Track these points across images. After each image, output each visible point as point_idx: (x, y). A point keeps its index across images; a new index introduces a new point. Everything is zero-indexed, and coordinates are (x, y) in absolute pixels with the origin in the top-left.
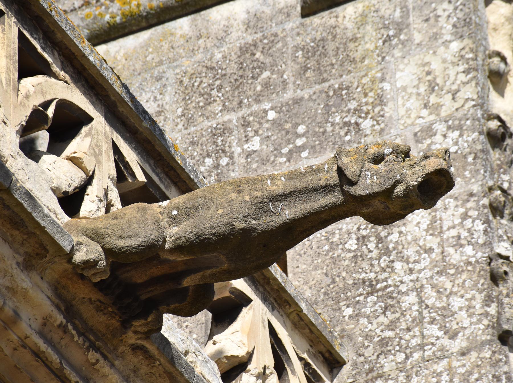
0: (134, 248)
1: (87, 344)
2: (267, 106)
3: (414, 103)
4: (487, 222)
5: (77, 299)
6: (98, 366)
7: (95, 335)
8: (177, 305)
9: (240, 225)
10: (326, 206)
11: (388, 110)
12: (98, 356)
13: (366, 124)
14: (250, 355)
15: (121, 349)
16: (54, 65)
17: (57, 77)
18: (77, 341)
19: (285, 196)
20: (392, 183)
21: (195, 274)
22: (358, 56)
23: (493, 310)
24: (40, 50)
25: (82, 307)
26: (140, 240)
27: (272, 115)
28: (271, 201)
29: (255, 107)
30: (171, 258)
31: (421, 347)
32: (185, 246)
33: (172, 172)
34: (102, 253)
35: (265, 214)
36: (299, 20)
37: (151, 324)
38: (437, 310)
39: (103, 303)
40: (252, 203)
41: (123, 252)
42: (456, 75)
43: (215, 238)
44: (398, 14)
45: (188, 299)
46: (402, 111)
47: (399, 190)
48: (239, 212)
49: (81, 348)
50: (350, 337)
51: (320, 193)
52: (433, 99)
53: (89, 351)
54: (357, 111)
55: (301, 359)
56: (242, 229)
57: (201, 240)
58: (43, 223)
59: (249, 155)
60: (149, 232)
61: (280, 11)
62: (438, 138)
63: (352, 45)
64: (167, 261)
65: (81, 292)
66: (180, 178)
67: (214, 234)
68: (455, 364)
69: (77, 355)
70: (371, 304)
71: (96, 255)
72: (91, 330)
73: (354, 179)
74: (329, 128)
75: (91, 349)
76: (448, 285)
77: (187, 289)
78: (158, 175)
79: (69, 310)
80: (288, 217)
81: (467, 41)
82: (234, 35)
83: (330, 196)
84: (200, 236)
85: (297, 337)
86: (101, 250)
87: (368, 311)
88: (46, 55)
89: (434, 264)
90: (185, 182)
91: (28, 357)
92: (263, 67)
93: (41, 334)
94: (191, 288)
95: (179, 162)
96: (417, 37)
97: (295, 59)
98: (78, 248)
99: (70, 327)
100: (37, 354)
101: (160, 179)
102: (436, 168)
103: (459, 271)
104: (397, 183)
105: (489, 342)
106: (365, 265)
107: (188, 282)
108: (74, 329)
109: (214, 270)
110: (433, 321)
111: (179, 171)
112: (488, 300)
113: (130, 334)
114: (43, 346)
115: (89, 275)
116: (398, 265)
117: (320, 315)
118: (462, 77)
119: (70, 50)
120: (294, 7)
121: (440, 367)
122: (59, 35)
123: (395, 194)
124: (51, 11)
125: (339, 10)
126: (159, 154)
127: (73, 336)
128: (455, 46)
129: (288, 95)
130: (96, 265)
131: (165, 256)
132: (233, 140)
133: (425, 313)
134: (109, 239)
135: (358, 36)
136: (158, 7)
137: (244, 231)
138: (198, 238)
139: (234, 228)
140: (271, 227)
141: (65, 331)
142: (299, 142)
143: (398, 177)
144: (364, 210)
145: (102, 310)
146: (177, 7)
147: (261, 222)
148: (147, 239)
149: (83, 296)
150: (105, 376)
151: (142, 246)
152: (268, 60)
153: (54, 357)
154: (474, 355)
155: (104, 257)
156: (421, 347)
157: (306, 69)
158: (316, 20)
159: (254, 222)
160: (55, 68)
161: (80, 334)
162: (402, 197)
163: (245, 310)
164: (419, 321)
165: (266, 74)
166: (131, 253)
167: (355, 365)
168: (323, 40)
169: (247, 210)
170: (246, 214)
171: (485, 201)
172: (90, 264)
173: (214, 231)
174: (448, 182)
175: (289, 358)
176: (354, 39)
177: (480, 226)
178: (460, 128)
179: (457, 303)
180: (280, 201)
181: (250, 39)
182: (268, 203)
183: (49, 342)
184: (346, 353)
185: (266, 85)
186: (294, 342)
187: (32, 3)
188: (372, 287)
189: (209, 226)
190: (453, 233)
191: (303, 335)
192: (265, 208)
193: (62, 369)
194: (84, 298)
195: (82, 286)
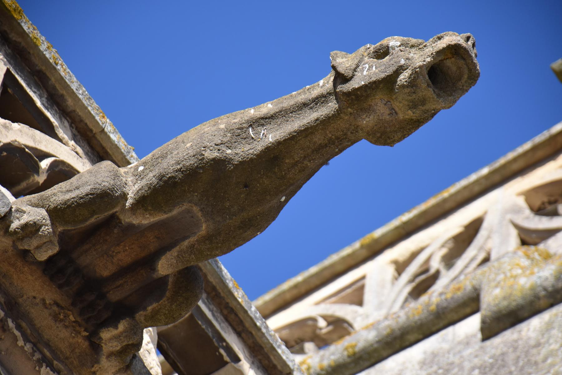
0: (81, 198)
1: (37, 356)
5: (25, 297)
7: (52, 351)
8: (155, 305)
9: (209, 155)
10: (317, 120)
16: (61, 131)
17: (60, 140)
18: (22, 347)
19: (269, 118)
20: (395, 69)
21: (170, 250)
22: (540, 358)
24: (39, 103)
25: (33, 310)
26: (89, 187)
28: (251, 126)
30: (135, 221)
32: (148, 196)
33: (232, 316)
34: (47, 217)
35: (244, 142)
36: (480, 344)
37: (124, 334)
39: (62, 308)
41: (69, 206)
43: (180, 176)
45: (168, 294)
47: (403, 77)
48: (210, 141)
49: (29, 359)
51: (311, 108)
53: (41, 366)
56: (214, 159)
57: (165, 182)
60: (101, 179)
61: (459, 343)
63: (534, 351)
64: (131, 227)
66: (244, 326)
67: (179, 170)
71: (38, 218)
72: (48, 345)
73: (349, 73)
75: (44, 365)
77: (163, 280)
78: (210, 310)
80: (271, 140)
83: (324, 109)
84: (164, 176)
86: (46, 214)
88: (48, 114)
90: (251, 333)
94: (171, 280)
95: (240, 300)
98: (18, 215)
99: (11, 324)
101: (214, 315)
102: (450, 43)
107: (165, 267)
108: (19, 327)
109: (193, 239)
111: (241, 315)
113: (104, 362)
115: (32, 248)
119: (86, 124)
120: (474, 336)
122: (70, 102)
123: (399, 82)
124: (57, 64)
126: (214, 288)
127: (16, 339)
130: (38, 230)
131: (128, 219)
134: (54, 198)
135: (542, 341)
136: (330, 366)
138: (160, 180)
139: (203, 159)
140: (250, 156)
143: (403, 62)
145: (61, 321)
146: (349, 363)
147: (238, 151)
148: (97, 186)
149: (34, 294)
151: (91, 194)
155: (49, 222)
158: (497, 341)
159: (229, 151)
160: (61, 133)
161: (26, 339)
162: (407, 86)
166: (79, 205)
168: (503, 354)
169: (220, 138)
170: (219, 142)
172: (31, 229)
173: (179, 167)
174: (470, 70)
176: (538, 345)
180: (263, 125)
182: (248, 128)
187: (31, 52)
189: (174, 162)
192: (244, 135)
194: (35, 298)
195: (30, 277)
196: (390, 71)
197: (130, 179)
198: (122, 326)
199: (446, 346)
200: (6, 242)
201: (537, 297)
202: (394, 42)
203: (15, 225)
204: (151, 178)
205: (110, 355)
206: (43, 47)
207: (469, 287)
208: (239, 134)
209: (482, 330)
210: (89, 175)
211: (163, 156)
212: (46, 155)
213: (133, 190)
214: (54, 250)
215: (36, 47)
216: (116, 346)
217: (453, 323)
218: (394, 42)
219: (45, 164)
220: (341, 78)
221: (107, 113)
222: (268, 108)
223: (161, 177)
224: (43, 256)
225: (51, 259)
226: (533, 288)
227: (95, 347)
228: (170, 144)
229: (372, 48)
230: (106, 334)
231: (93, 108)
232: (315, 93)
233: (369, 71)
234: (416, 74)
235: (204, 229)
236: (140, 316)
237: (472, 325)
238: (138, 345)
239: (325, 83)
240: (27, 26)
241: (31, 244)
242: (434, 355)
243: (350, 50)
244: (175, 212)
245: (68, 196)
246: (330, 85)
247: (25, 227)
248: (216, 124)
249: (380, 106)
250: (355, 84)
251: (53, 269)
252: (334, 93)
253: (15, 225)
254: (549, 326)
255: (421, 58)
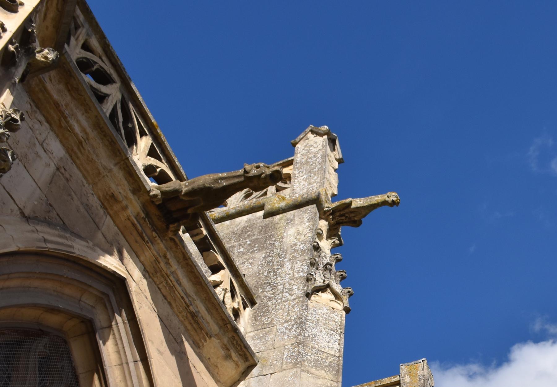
2: (247, 240)
3: (292, 238)
4: (308, 266)
6: (156, 239)
9: (207, 185)
11: (284, 240)
12: (156, 235)
13: (277, 244)
14: (221, 282)
15: (166, 238)
17: (163, 163)
22: (278, 227)
23: (305, 288)
24: (159, 152)
27: (248, 242)
29: (244, 241)
30: (184, 198)
31: (281, 299)
38: (288, 289)
40: (213, 179)
42: (307, 231)
44: (292, 217)
46: (288, 240)
47: (263, 176)
50: (260, 297)
52: (298, 237)
54: (275, 241)
55: (241, 296)
58: (140, 176)
59: (239, 252)
62: (298, 246)
64: (182, 200)
65: (153, 211)
68: (291, 302)
69: (149, 232)
70: (268, 288)
73: (248, 171)
74: (265, 245)
76: (293, 283)
79: (147, 214)
81: (311, 223)
82: (242, 224)
85: (241, 290)
87: (267, 290)
89: (290, 277)
91: (130, 225)
92: (248, 231)
93: (136, 218)
96: (296, 222)
97: (259, 229)
99: (147, 220)
100: (134, 225)
103: (297, 279)
104: (263, 173)
105: (303, 297)
106: (269, 279)
107: (190, 211)
108: (149, 221)
110: (286, 292)
112: (305, 286)
113: (169, 232)
114: (136, 222)
116: (279, 278)
117: (250, 282)
118: (308, 231)
121: (285, 304)
122: (167, 152)
125: (275, 217)
128: (307, 224)
129: (255, 237)
132: (235, 249)
133: (285, 290)
137: (208, 187)
141: (145, 221)
142: (255, 249)
144: (251, 185)
150: (158, 244)
152: (250, 230)
153: (140, 228)
154: (297, 300)
156: (281, 299)
157: (261, 231)
158: (267, 220)
160: (163, 161)
161: (150, 224)
163: (222, 271)
164: (282, 292)
165: (249, 233)
167: (260, 304)
171: (309, 261)
172: (155, 196)
175: (236, 293)
176: (278, 223)
177: (306, 267)
178: (305, 243)
179: (295, 287)
181: (246, 225)
183: (139, 223)
184: (258, 301)
185: (249, 235)
186: (239, 290)
188: (269, 284)
190: (298, 269)
191: (243, 290)
193: (142, 233)
196: (260, 173)
197: (184, 186)
198: (176, 225)
199: (253, 218)
200: (148, 198)
201: (279, 210)
202: (262, 165)
203: (151, 194)
204: (190, 188)
205: (171, 231)
206: (162, 137)
207: (262, 202)
208: (216, 181)
209: (264, 216)
210: (174, 184)
211: (194, 182)
212: (158, 167)
213: (184, 190)
214: (160, 202)
215: (160, 136)
216: (173, 229)
217: (256, 212)
218: (262, 165)
219: (158, 170)
220: (246, 172)
221: (176, 156)
222: (225, 175)
223: (193, 189)
224: (157, 203)
225: (159, 205)
226: (279, 207)
227: (168, 228)
228: (196, 179)
229: (256, 165)
230: (171, 226)
231: (173, 155)
232: (238, 174)
233: (254, 172)
234: (266, 176)
235: (202, 204)
236: (181, 222)
237: (261, 213)
238: (179, 230)
239: (241, 171)
240: (159, 131)
241: (155, 200)
242: (250, 220)
243: (249, 163)
244: (195, 198)
245: (167, 189)
246: (243, 172)
247: (154, 195)
248: (209, 176)
249: (255, 182)
250: (251, 175)
251: (159, 207)
252: (243, 175)
253: (151, 194)
254: (281, 219)
255: (268, 171)
